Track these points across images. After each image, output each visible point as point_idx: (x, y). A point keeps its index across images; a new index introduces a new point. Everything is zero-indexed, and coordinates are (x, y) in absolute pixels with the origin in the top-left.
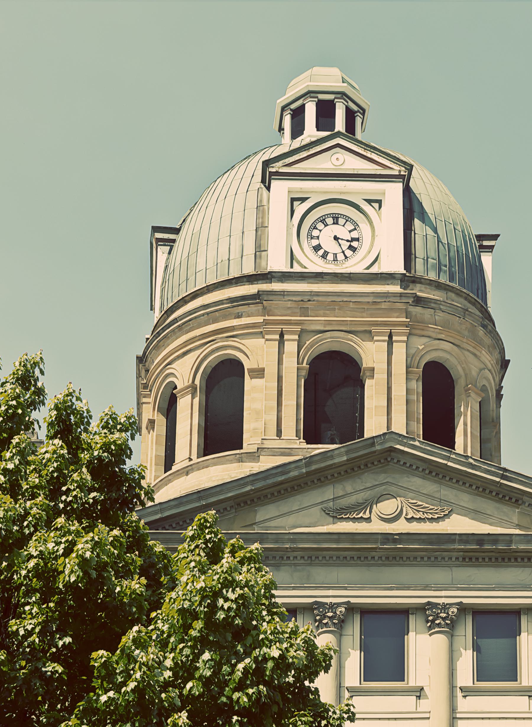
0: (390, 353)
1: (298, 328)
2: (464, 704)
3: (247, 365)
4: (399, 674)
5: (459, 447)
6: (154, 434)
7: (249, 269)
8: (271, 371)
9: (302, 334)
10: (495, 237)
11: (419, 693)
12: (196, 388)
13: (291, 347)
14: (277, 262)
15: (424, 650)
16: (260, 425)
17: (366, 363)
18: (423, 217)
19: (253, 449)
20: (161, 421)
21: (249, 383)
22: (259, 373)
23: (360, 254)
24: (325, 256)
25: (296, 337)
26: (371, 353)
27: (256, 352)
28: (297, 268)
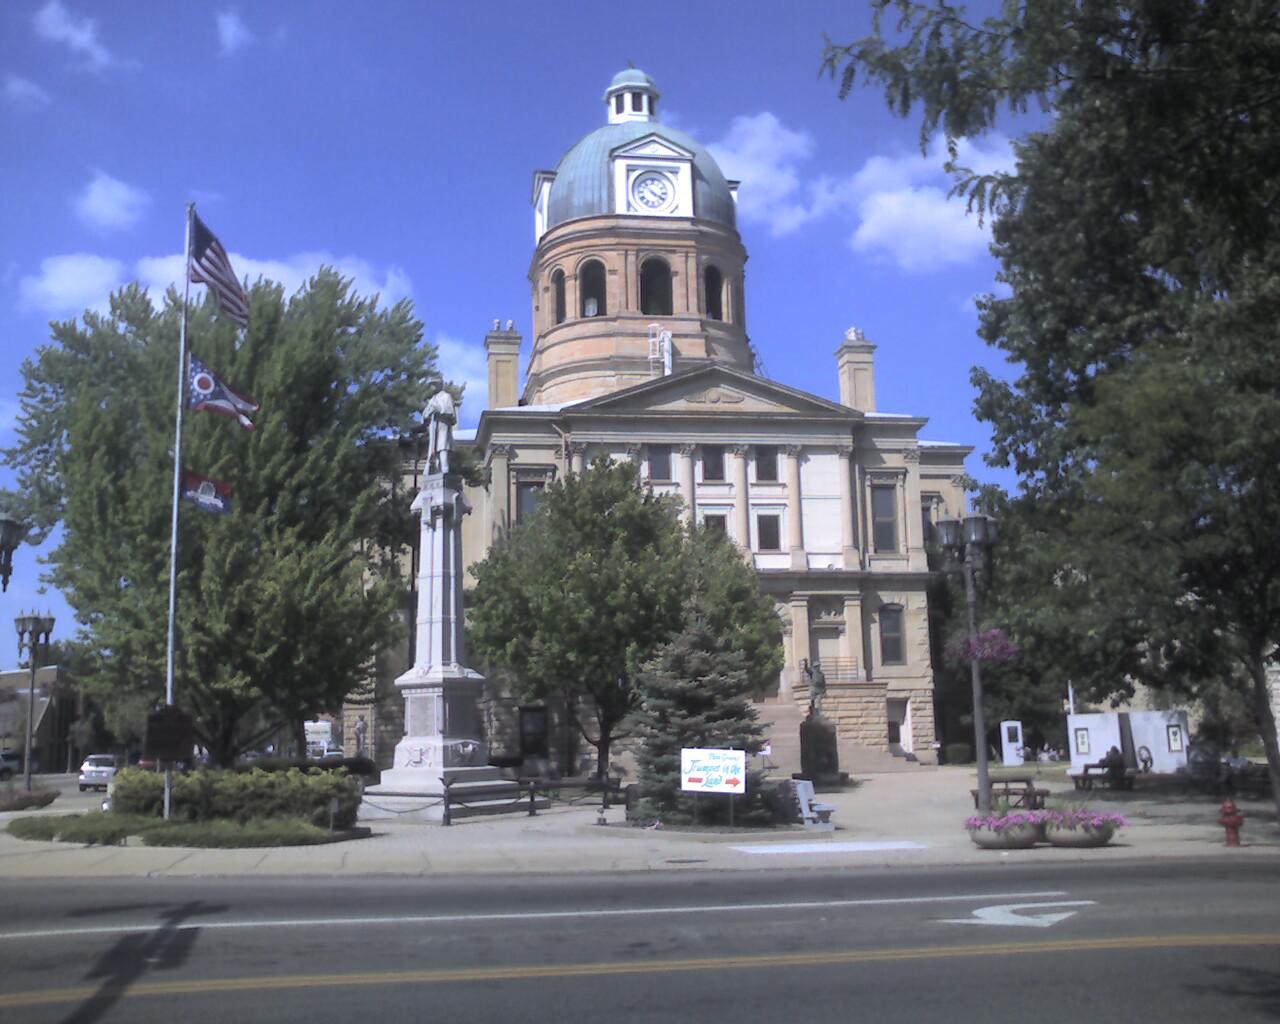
0: (686, 262)
1: (635, 248)
2: (753, 491)
3: (608, 267)
4: (721, 477)
5: (725, 319)
6: (549, 293)
7: (605, 211)
8: (621, 270)
9: (638, 251)
10: (738, 182)
11: (784, 485)
12: (987, 689)
13: (632, 258)
14: (621, 209)
15: (732, 464)
16: (617, 302)
17: (673, 269)
18: (702, 178)
19: (613, 316)
20: (553, 287)
21: (609, 278)
22: (613, 272)
23: (667, 203)
24: (647, 203)
25: (858, 602)
26: (676, 262)
27: (612, 260)
28: (631, 213)
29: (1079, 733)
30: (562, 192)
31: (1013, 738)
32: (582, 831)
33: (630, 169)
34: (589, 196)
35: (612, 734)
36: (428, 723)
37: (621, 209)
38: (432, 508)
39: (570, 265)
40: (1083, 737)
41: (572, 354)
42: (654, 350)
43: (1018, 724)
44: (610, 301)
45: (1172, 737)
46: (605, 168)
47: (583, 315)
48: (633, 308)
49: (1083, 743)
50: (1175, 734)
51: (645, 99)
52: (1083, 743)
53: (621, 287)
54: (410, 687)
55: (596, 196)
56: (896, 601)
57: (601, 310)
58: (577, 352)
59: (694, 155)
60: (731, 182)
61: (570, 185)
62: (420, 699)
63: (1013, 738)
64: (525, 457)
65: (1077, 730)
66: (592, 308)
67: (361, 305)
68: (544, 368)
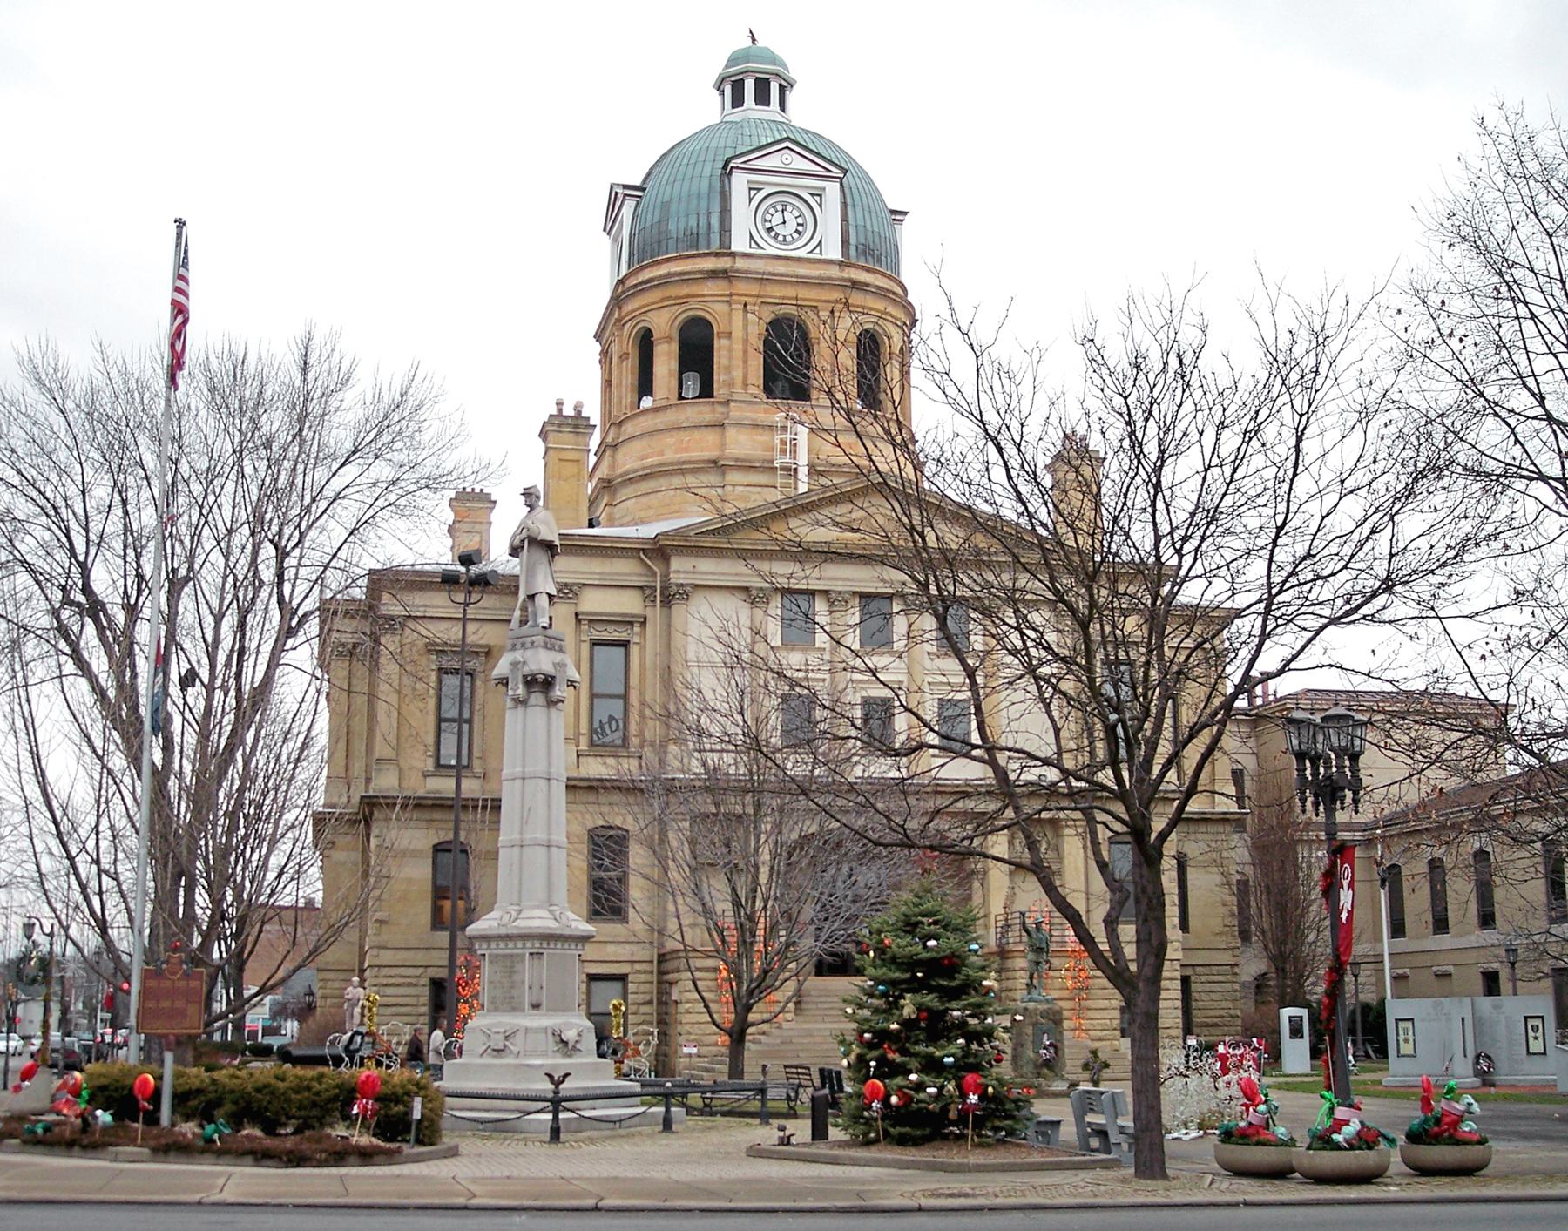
7: (715, 247)
29: (1531, 1022)
30: (652, 216)
31: (1296, 1032)
32: (756, 1152)
33: (754, 188)
34: (693, 223)
35: (751, 1017)
36: (515, 993)
37: (739, 244)
38: (525, 677)
39: (664, 324)
40: (1406, 1031)
41: (662, 453)
42: (783, 452)
43: (1304, 1012)
44: (719, 377)
45: (1531, 1033)
46: (717, 184)
47: (681, 398)
48: (757, 390)
49: (1406, 1041)
50: (1535, 1029)
51: (750, 85)
52: (1406, 1041)
53: (739, 358)
54: (486, 938)
55: (703, 222)
56: (618, 822)
57: (706, 390)
58: (670, 450)
59: (845, 172)
60: (894, 212)
61: (665, 206)
62: (505, 956)
63: (1296, 1032)
64: (593, 602)
65: (1397, 1021)
66: (692, 385)
67: (1075, 455)
68: (620, 471)
